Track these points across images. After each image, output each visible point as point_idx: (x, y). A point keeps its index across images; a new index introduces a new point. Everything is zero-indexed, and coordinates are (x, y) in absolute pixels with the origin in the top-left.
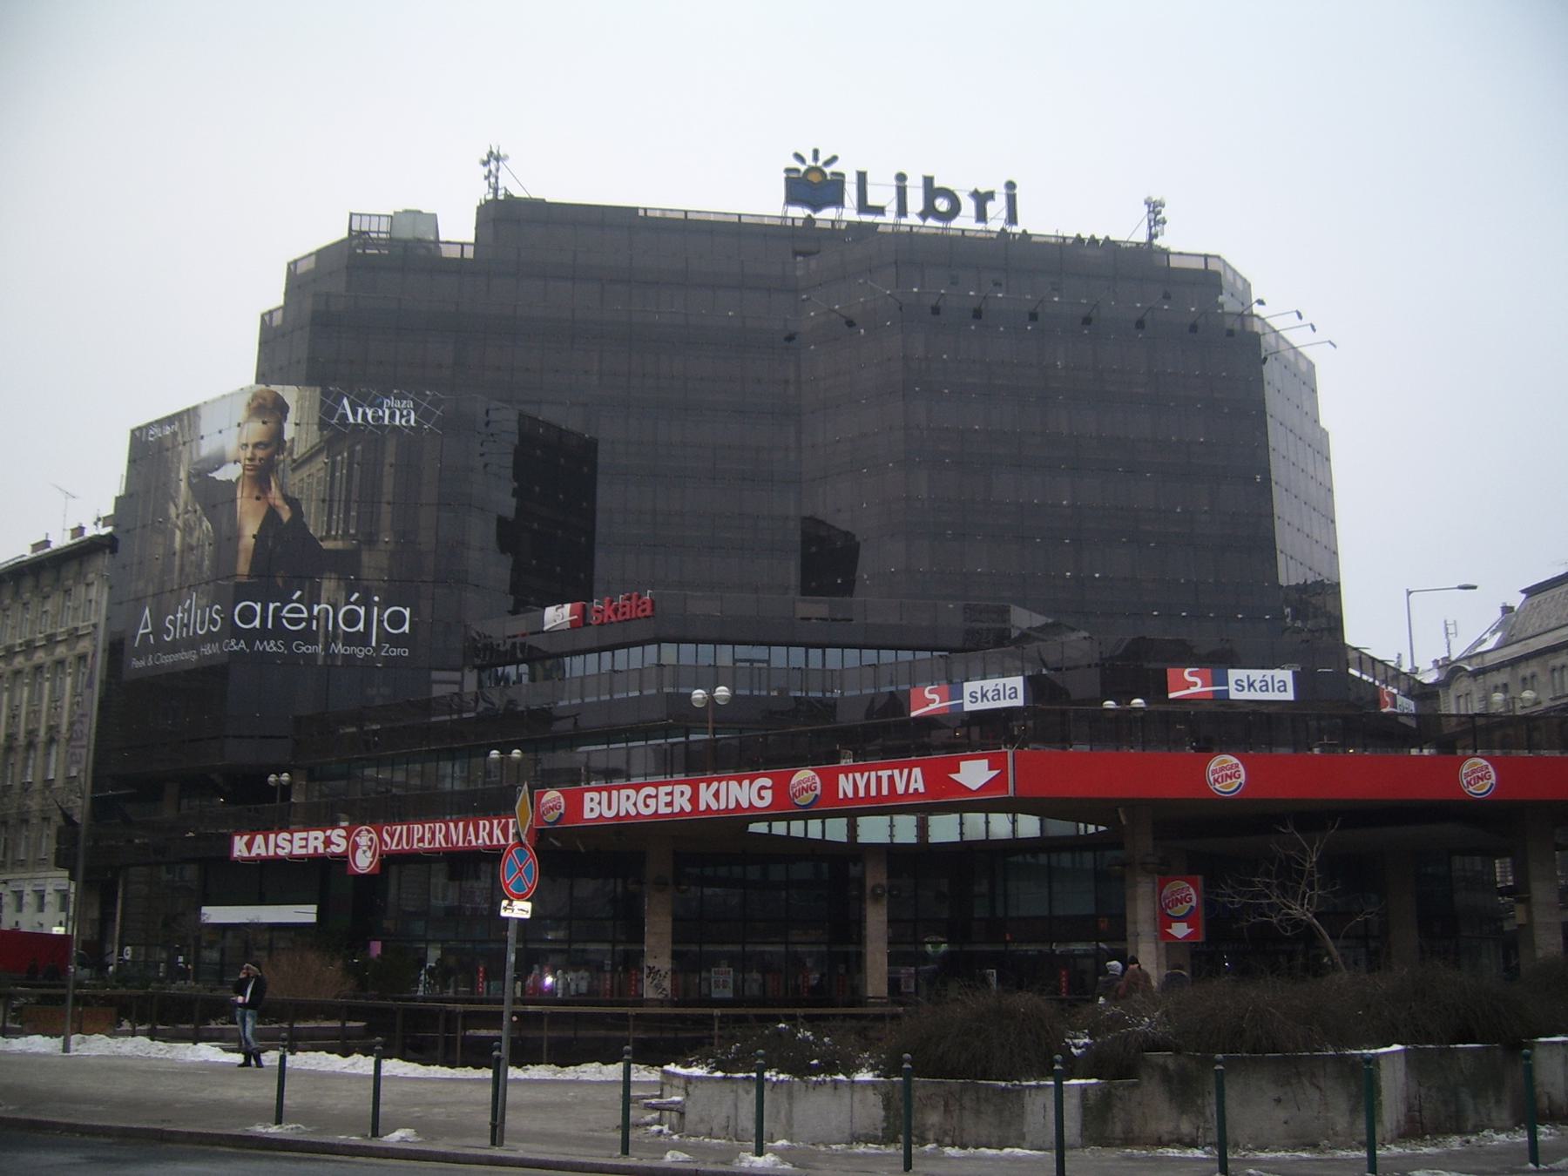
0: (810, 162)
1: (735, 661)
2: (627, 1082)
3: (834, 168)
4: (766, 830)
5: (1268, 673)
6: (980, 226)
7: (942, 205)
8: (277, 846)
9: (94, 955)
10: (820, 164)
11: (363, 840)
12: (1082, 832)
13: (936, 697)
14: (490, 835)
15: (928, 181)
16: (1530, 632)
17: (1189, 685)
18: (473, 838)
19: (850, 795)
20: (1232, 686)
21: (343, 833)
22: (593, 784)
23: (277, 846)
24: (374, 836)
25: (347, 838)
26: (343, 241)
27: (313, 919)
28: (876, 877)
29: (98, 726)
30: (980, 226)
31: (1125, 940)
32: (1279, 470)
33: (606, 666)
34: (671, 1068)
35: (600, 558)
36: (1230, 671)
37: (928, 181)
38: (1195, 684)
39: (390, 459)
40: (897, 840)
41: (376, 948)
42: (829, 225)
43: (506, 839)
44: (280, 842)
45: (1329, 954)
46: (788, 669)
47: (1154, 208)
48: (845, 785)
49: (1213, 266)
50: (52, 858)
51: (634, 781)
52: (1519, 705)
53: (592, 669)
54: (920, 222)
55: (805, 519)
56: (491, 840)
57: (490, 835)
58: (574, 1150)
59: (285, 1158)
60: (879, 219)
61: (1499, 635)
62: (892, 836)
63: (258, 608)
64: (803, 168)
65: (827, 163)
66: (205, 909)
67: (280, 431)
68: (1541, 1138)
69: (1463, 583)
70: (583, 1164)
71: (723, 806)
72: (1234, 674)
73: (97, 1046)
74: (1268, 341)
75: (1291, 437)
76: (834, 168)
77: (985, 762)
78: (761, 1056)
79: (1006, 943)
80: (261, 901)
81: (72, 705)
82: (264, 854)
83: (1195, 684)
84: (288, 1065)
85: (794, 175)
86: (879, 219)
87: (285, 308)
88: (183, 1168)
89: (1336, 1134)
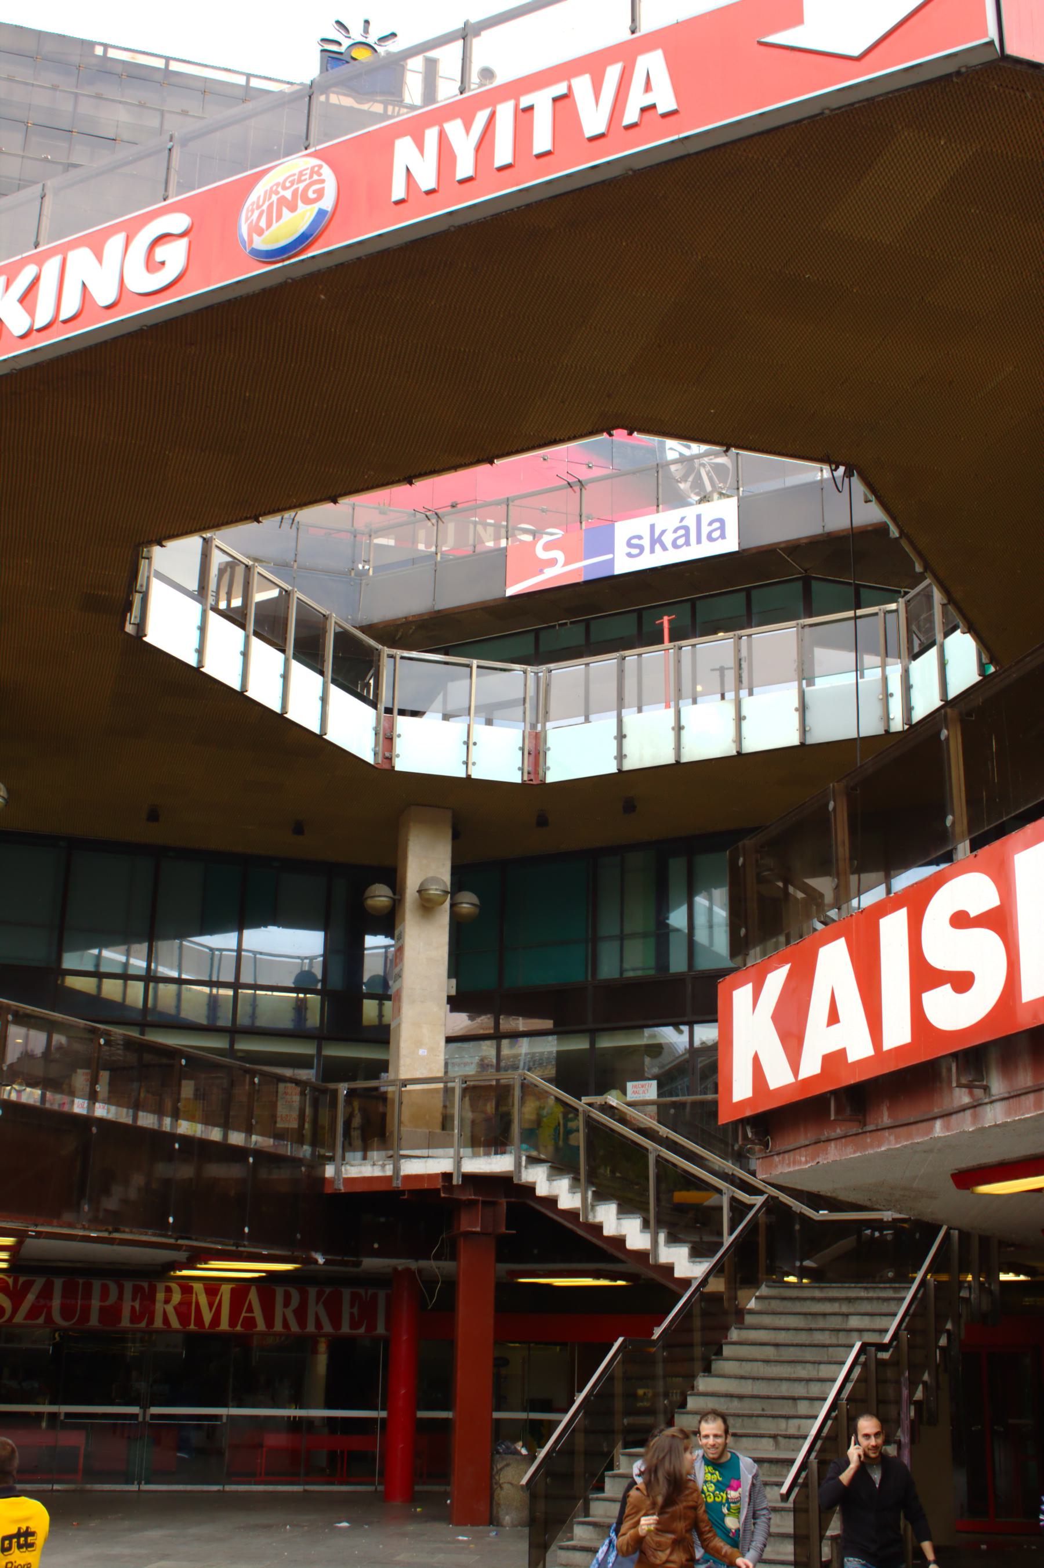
0: (357, 35)
4: (129, 1121)
8: (924, 976)
10: (372, 40)
13: (559, 555)
18: (258, 1314)
22: (234, 1171)
23: (924, 976)
26: (115, 1002)
27: (192, 1083)
28: (427, 863)
32: (854, 1201)
36: (734, 548)
38: (553, 562)
39: (456, 1131)
41: (303, 1169)
44: (944, 948)
45: (806, 1162)
47: (712, 670)
50: (71, 1098)
52: (166, 1307)
56: (302, 1322)
61: (467, 1099)
62: (621, 757)
64: (346, 43)
65: (383, 39)
66: (841, 943)
69: (507, 673)
71: (42, 318)
76: (461, 1022)
80: (669, 1313)
82: (859, 1048)
83: (553, 562)
84: (160, 993)
85: (334, 48)
88: (498, 1170)
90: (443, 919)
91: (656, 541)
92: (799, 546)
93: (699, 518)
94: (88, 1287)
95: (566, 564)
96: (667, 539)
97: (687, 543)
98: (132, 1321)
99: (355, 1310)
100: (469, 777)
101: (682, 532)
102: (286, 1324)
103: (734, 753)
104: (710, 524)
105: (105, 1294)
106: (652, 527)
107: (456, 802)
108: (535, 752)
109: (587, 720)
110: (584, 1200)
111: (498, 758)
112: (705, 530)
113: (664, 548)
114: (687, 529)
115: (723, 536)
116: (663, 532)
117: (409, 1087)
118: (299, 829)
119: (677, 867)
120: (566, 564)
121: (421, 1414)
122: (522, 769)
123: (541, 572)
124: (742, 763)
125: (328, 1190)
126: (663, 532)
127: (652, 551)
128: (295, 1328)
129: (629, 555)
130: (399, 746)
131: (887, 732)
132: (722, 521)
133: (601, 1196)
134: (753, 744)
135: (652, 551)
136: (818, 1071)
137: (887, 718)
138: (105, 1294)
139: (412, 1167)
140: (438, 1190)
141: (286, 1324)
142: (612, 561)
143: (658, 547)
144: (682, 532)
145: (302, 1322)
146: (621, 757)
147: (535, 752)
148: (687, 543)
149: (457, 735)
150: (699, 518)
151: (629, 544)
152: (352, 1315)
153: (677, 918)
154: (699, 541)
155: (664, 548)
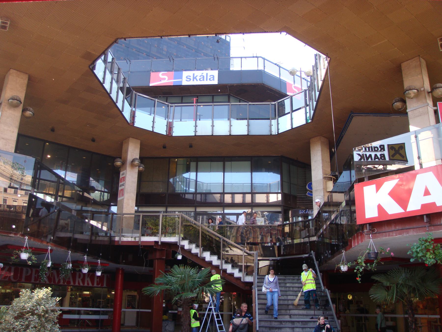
2: (158, 259)
5: (204, 72)
6: (194, 222)
9: (80, 296)
17: (161, 79)
19: (372, 298)
29: (129, 265)
30: (194, 222)
34: (327, 290)
35: (230, 163)
38: (164, 79)
42: (231, 99)
43: (93, 283)
46: (213, 118)
48: (168, 210)
51: (195, 205)
55: (16, 152)
56: (83, 283)
59: (4, 236)
62: (196, 131)
67: (159, 250)
72: (185, 74)
73: (240, 128)
77: (94, 71)
79: (327, 220)
80: (156, 82)
83: (164, 79)
87: (353, 151)
90: (136, 170)
91: (194, 78)
92: (233, 86)
93: (207, 74)
94: (22, 270)
95: (168, 80)
96: (198, 78)
97: (203, 80)
98: (35, 281)
99: (98, 280)
100: (153, 131)
101: (202, 77)
102: (79, 283)
103: (229, 134)
104: (210, 76)
105: (27, 272)
106: (194, 74)
107: (146, 137)
108: (170, 127)
109: (181, 121)
110: (200, 250)
111: (161, 128)
112: (209, 77)
113: (197, 80)
114: (204, 76)
115: (213, 80)
116: (197, 76)
117: (125, 216)
118: (93, 140)
119: (193, 164)
120: (168, 80)
121: (150, 311)
122: (166, 131)
123: (161, 81)
124: (230, 137)
125: (116, 244)
126: (197, 76)
127: (193, 80)
128: (81, 284)
129: (187, 80)
130: (136, 119)
131: (271, 134)
132: (213, 76)
133: (205, 250)
134: (234, 133)
135: (193, 80)
136: (390, 213)
137: (271, 131)
138: (27, 272)
139: (125, 239)
140: (153, 246)
141: (79, 283)
142: (182, 81)
143: (195, 80)
144: (202, 77)
145: (83, 283)
146: (196, 131)
147: (170, 127)
148: (203, 80)
149: (147, 119)
150: (207, 74)
151: (187, 77)
152: (97, 281)
153: (171, 180)
154: (207, 80)
155: (197, 80)
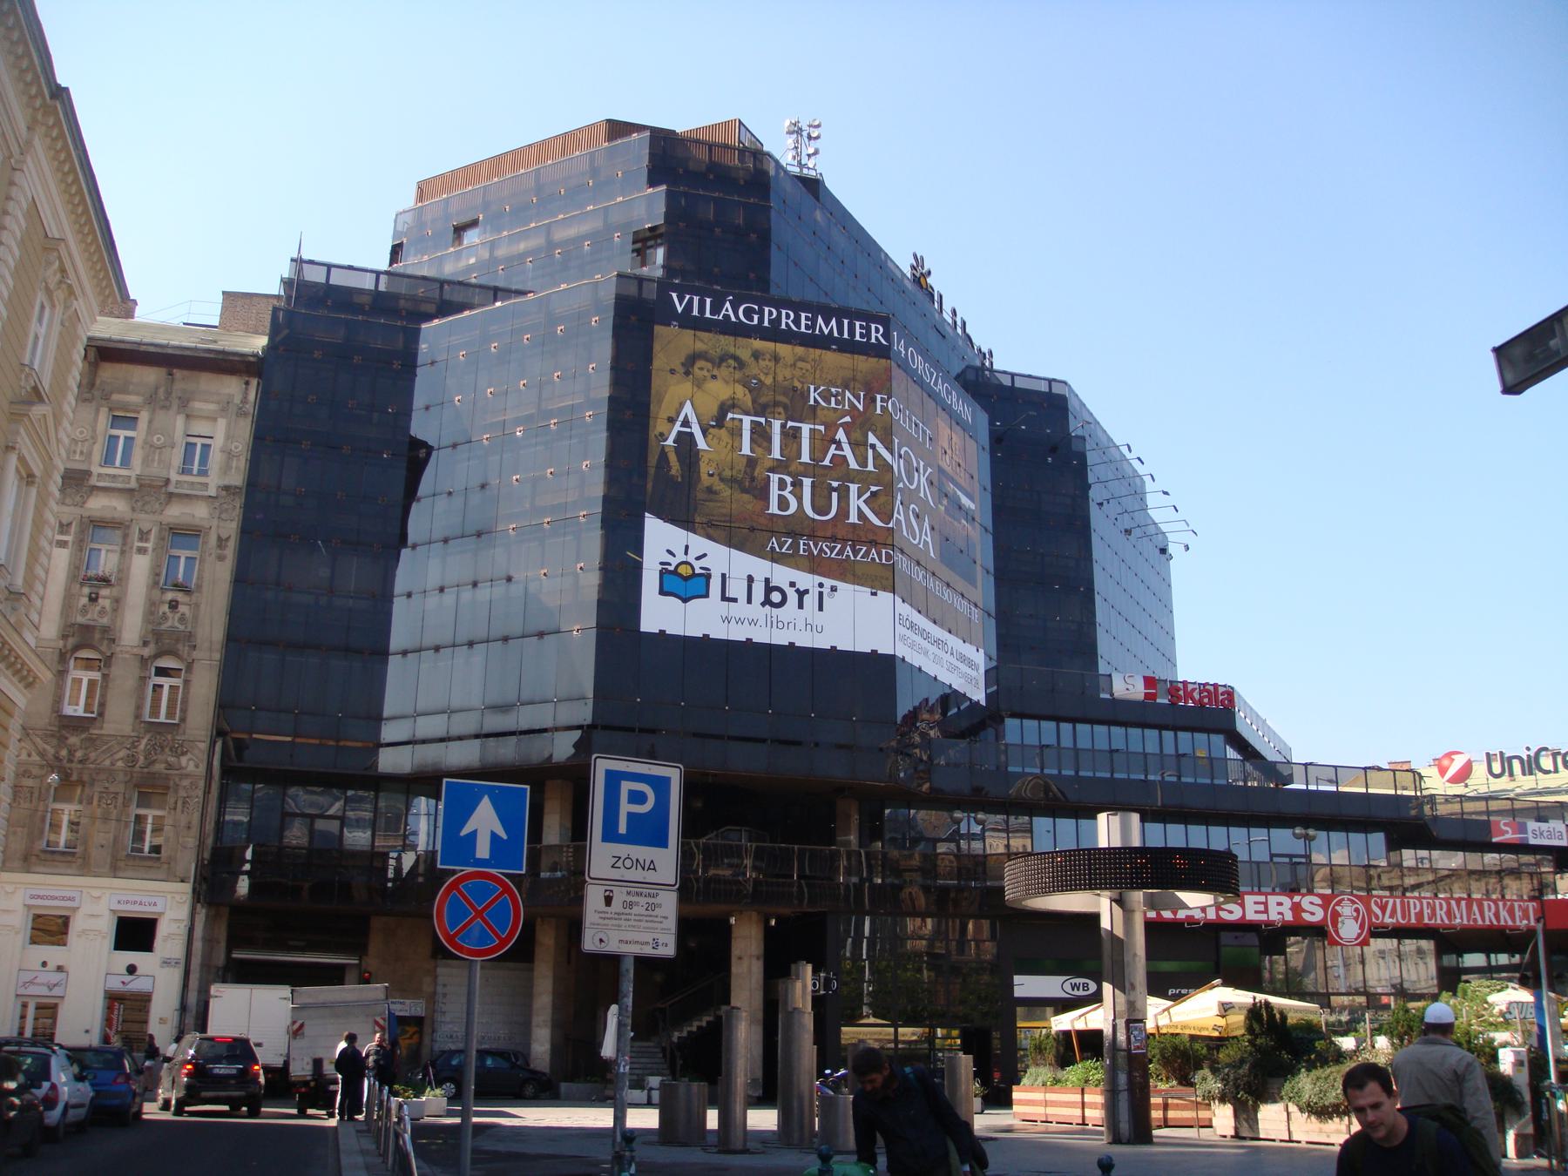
0: (681, 557)
1: (1272, 856)
3: (703, 563)
7: (776, 597)
11: (1346, 910)
12: (1153, 1100)
14: (1497, 915)
15: (767, 581)
16: (513, 739)
20: (1530, 835)
21: (1318, 901)
24: (1361, 907)
25: (1325, 907)
31: (615, 959)
33: (1169, 749)
37: (767, 581)
40: (1191, 845)
49: (1056, 389)
53: (1031, 739)
54: (1222, 1022)
57: (1497, 915)
58: (48, 213)
60: (35, 319)
63: (708, 315)
65: (698, 558)
68: (1225, 951)
70: (12, 534)
74: (1072, 404)
75: (1113, 612)
78: (12, 1107)
81: (152, 606)
86: (35, 319)
89: (1531, 874)
